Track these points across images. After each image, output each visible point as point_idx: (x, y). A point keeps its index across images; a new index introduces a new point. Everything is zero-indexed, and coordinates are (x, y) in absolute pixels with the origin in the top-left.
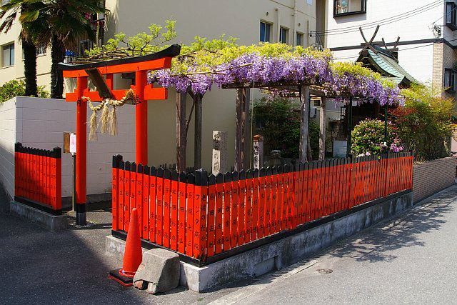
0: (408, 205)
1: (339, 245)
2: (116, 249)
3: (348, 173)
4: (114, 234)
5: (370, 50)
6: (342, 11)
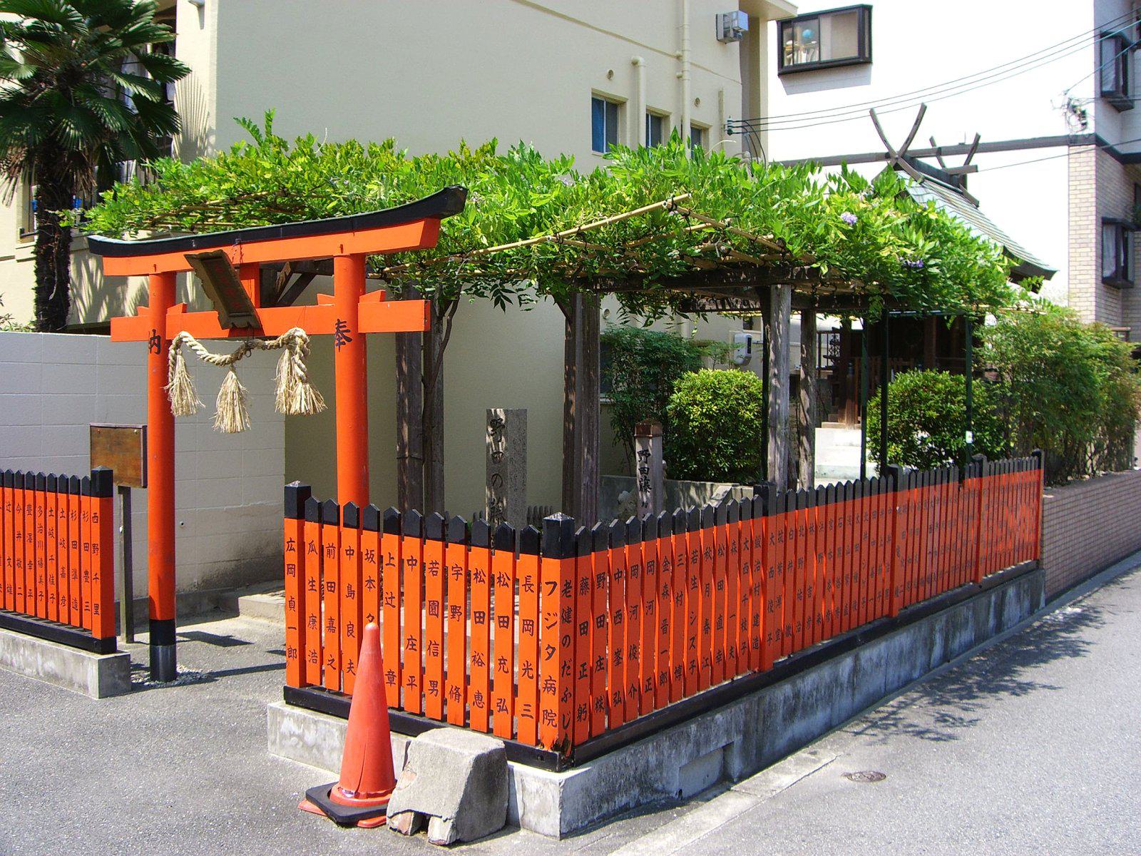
0: (1034, 606)
1: (861, 709)
2: (301, 737)
3: (890, 517)
4: (292, 697)
5: (902, 174)
6: (803, 58)
